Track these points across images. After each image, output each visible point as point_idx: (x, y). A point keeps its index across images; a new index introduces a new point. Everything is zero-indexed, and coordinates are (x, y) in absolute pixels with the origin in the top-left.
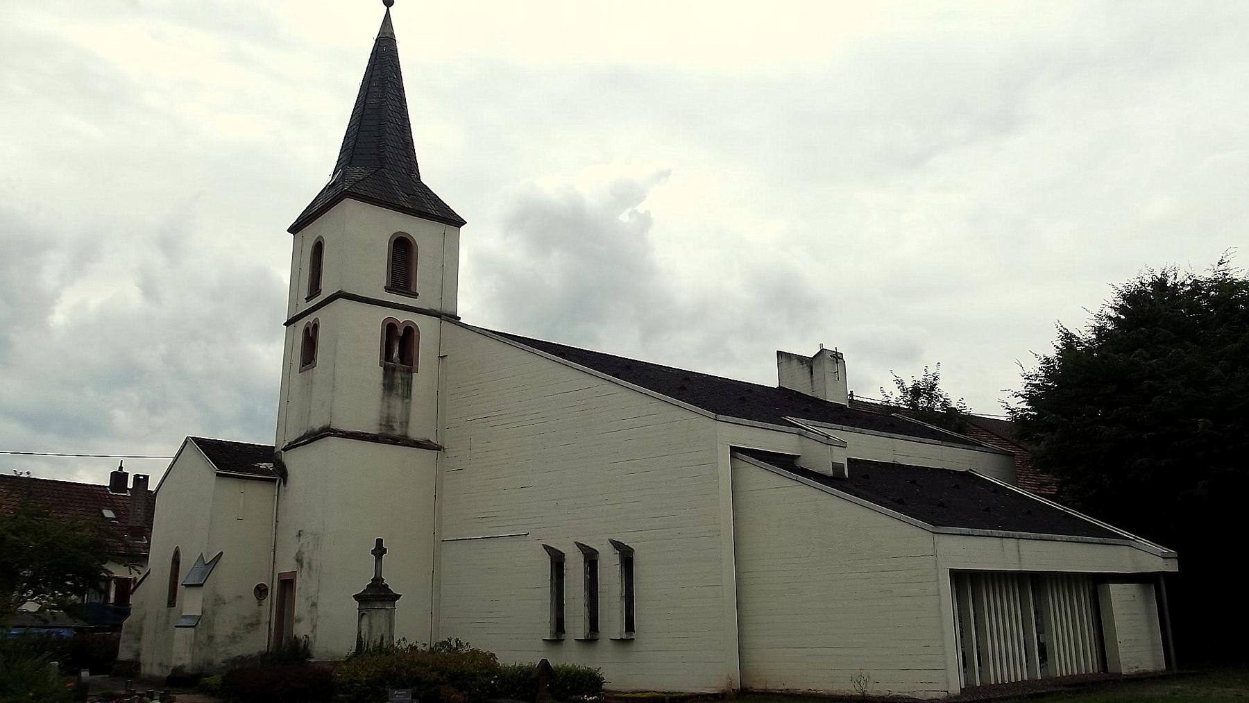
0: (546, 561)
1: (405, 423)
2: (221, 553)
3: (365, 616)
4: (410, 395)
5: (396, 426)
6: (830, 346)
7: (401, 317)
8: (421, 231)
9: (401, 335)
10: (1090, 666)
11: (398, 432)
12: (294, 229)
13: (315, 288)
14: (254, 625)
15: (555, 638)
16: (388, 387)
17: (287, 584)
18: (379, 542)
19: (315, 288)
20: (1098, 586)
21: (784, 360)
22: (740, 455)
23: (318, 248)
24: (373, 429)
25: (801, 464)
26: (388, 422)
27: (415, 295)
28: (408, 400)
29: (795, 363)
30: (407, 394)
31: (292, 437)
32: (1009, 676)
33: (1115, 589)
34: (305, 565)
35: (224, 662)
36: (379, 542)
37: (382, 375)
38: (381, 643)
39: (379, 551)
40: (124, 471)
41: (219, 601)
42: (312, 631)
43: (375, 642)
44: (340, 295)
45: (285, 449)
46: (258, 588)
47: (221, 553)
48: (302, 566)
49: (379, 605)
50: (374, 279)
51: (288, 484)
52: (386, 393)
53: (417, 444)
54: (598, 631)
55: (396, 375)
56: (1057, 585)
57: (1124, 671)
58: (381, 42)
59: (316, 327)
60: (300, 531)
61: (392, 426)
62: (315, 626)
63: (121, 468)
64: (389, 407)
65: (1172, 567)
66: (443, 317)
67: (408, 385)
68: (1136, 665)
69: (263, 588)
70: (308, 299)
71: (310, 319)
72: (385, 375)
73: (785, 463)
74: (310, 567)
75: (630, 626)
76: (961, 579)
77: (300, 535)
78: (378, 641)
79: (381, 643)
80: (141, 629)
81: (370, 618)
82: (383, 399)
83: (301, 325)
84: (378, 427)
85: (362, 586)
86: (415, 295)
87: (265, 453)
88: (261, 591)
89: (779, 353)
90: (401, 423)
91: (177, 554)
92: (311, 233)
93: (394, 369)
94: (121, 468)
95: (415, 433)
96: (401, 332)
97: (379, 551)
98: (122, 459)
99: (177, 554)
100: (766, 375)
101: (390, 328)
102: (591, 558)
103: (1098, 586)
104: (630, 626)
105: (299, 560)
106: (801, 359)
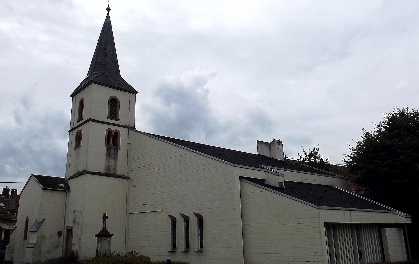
0: (169, 221)
1: (115, 169)
2: (44, 219)
4: (117, 157)
5: (112, 170)
7: (114, 128)
8: (121, 96)
9: (113, 135)
11: (112, 172)
12: (72, 95)
14: (56, 247)
16: (109, 155)
17: (70, 231)
18: (105, 214)
23: (82, 102)
24: (102, 171)
25: (267, 183)
26: (108, 168)
27: (119, 120)
28: (116, 160)
29: (264, 145)
30: (116, 158)
31: (72, 174)
33: (387, 230)
34: (77, 224)
36: (105, 214)
37: (106, 151)
38: (106, 253)
39: (105, 217)
42: (79, 249)
43: (103, 253)
45: (69, 179)
46: (58, 232)
47: (44, 219)
48: (75, 223)
49: (105, 238)
51: (70, 192)
52: (108, 157)
53: (120, 177)
55: (111, 150)
59: (81, 132)
62: (80, 247)
63: (7, 187)
64: (109, 163)
65: (409, 221)
66: (130, 128)
67: (116, 154)
69: (60, 232)
70: (78, 122)
71: (78, 129)
72: (107, 151)
73: (261, 182)
75: (201, 245)
76: (328, 226)
78: (104, 253)
79: (106, 253)
81: (101, 244)
82: (106, 160)
83: (75, 131)
84: (104, 170)
86: (119, 120)
88: (60, 233)
90: (113, 169)
91: (27, 219)
92: (79, 96)
93: (111, 148)
94: (7, 187)
95: (119, 172)
96: (113, 134)
97: (105, 217)
99: (27, 219)
101: (109, 132)
102: (186, 220)
105: (74, 221)
106: (266, 143)
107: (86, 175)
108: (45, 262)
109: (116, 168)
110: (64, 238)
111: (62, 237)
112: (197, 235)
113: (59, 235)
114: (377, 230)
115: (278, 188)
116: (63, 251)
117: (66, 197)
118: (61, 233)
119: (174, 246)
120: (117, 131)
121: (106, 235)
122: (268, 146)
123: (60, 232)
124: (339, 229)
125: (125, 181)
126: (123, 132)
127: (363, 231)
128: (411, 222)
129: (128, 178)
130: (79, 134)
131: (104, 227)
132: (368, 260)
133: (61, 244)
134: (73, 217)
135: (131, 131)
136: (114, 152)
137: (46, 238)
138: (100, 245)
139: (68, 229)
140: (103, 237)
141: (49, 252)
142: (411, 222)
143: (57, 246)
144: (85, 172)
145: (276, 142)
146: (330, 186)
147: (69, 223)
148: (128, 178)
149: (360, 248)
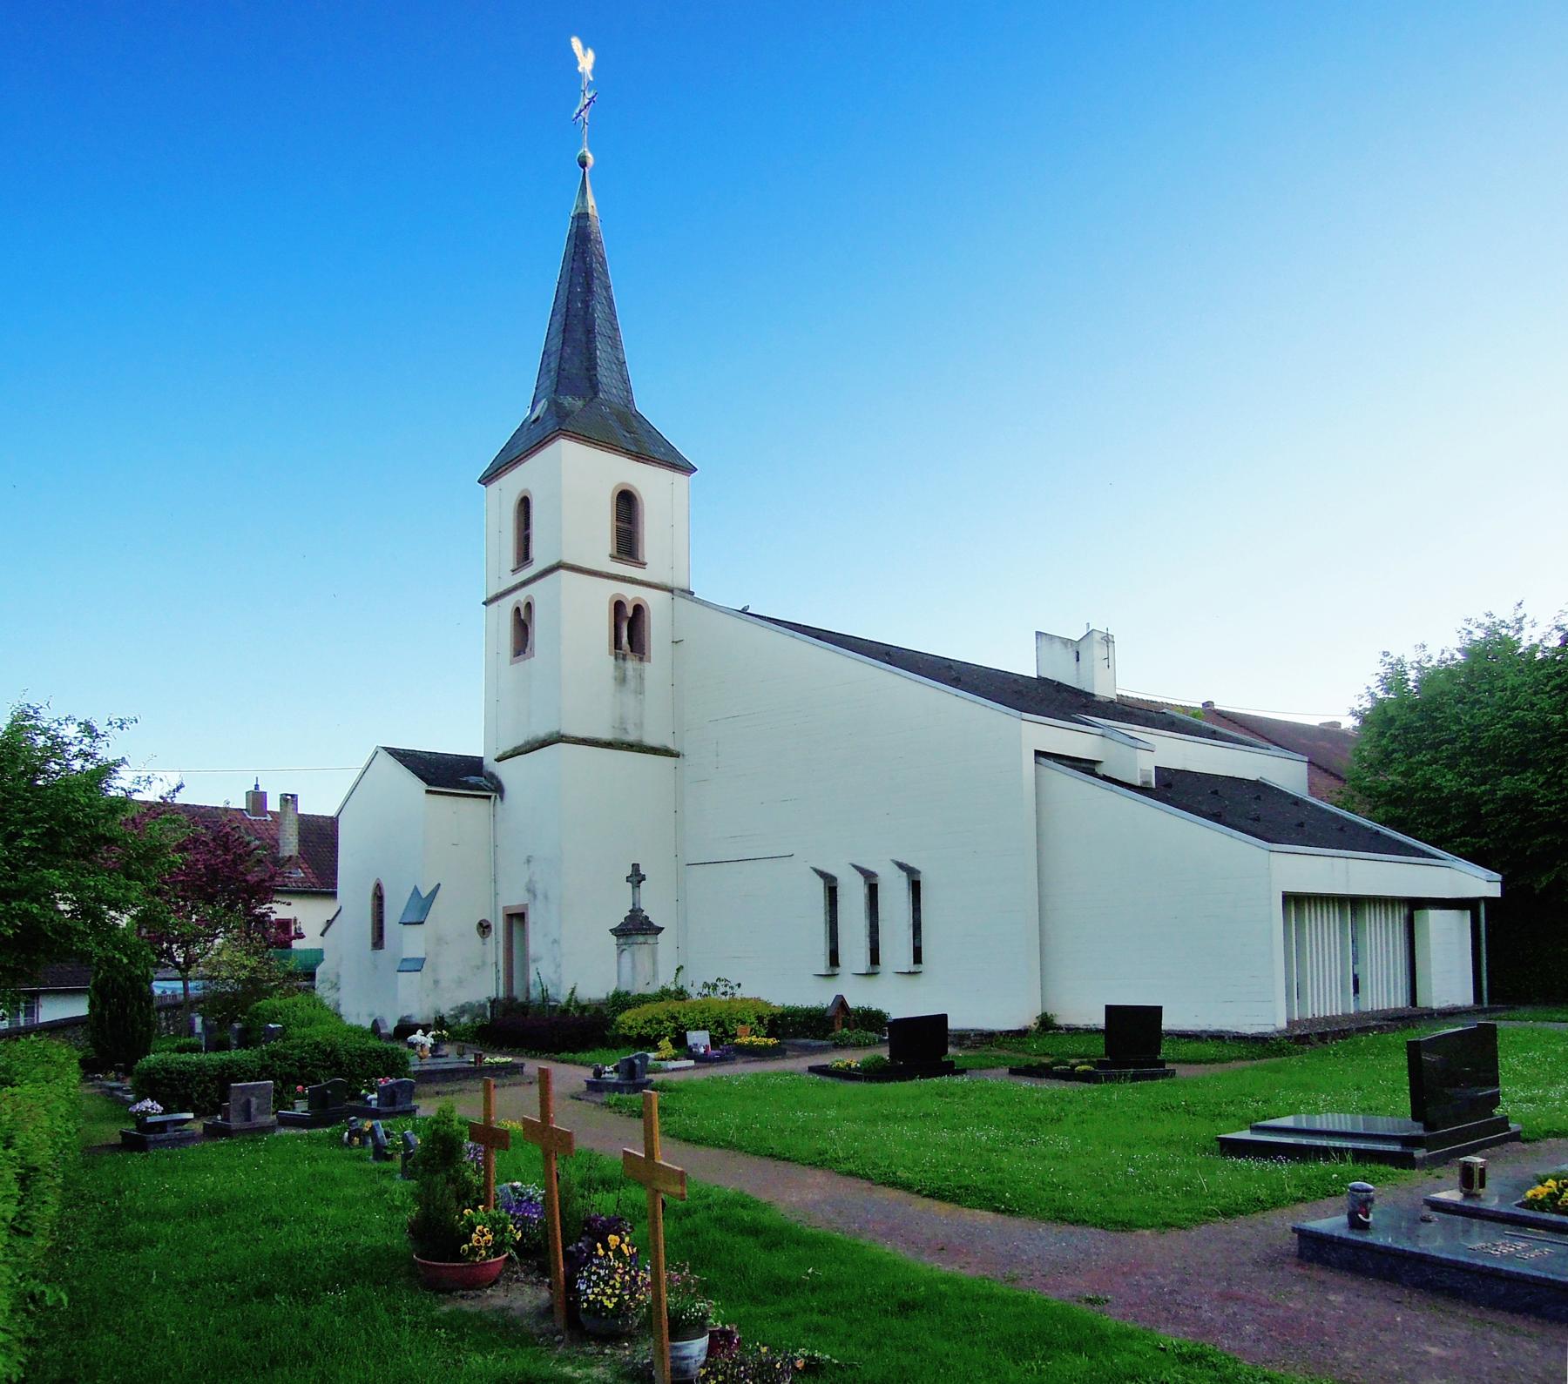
0: (819, 885)
1: (640, 725)
2: (439, 885)
3: (625, 952)
5: (631, 728)
6: (1099, 626)
7: (631, 594)
8: (647, 480)
9: (630, 616)
10: (1399, 1001)
13: (524, 554)
14: (481, 967)
15: (830, 973)
17: (517, 918)
18: (636, 867)
19: (524, 554)
20: (1415, 912)
21: (1044, 642)
22: (1042, 760)
25: (1100, 770)
27: (642, 565)
28: (641, 697)
29: (1058, 646)
30: (640, 691)
31: (507, 747)
32: (1331, 1009)
33: (1434, 916)
34: (540, 897)
35: (452, 1010)
36: (636, 867)
39: (636, 877)
40: (261, 789)
41: (440, 940)
42: (555, 972)
44: (559, 566)
46: (480, 924)
47: (439, 885)
48: (535, 896)
49: (641, 939)
50: (597, 544)
51: (506, 800)
54: (878, 964)
56: (1375, 907)
57: (1435, 1005)
58: (581, 220)
60: (530, 856)
61: (625, 729)
62: (559, 966)
63: (257, 786)
65: (1495, 891)
66: (676, 592)
68: (1446, 999)
69: (485, 925)
71: (520, 596)
73: (1086, 767)
74: (546, 897)
75: (917, 958)
76: (1295, 901)
77: (528, 861)
80: (338, 976)
81: (633, 955)
83: (508, 604)
85: (618, 920)
86: (642, 565)
87: (473, 765)
88: (484, 928)
89: (1038, 633)
90: (635, 724)
91: (378, 887)
92: (514, 483)
93: (624, 658)
94: (257, 786)
96: (630, 612)
97: (636, 877)
98: (258, 774)
99: (378, 887)
100: (1023, 664)
103: (1415, 912)
104: (917, 958)
105: (531, 890)
106: (1067, 642)
107: (560, 744)
108: (452, 1013)
109: (642, 724)
110: (497, 943)
111: (491, 939)
112: (864, 938)
113: (484, 934)
114: (1402, 915)
115: (1138, 787)
116: (498, 979)
117: (492, 817)
118: (488, 926)
119: (834, 959)
120: (639, 603)
121: (646, 930)
122: (1070, 650)
123: (485, 925)
124: (1310, 910)
125: (669, 761)
126: (654, 601)
127: (1367, 916)
128: (1500, 896)
129: (676, 755)
130: (525, 613)
131: (637, 907)
132: (1375, 1001)
133: (491, 959)
134: (527, 879)
135: (681, 603)
136: (634, 670)
137: (447, 943)
138: (629, 960)
139: (508, 915)
140: (637, 934)
141: (460, 983)
142: (1500, 896)
143: (480, 964)
144: (560, 739)
145: (1097, 637)
146: (1258, 781)
147: (513, 898)
148: (676, 755)
149: (1355, 966)
